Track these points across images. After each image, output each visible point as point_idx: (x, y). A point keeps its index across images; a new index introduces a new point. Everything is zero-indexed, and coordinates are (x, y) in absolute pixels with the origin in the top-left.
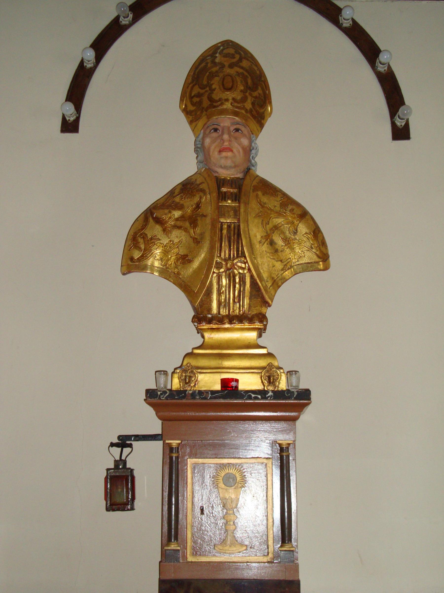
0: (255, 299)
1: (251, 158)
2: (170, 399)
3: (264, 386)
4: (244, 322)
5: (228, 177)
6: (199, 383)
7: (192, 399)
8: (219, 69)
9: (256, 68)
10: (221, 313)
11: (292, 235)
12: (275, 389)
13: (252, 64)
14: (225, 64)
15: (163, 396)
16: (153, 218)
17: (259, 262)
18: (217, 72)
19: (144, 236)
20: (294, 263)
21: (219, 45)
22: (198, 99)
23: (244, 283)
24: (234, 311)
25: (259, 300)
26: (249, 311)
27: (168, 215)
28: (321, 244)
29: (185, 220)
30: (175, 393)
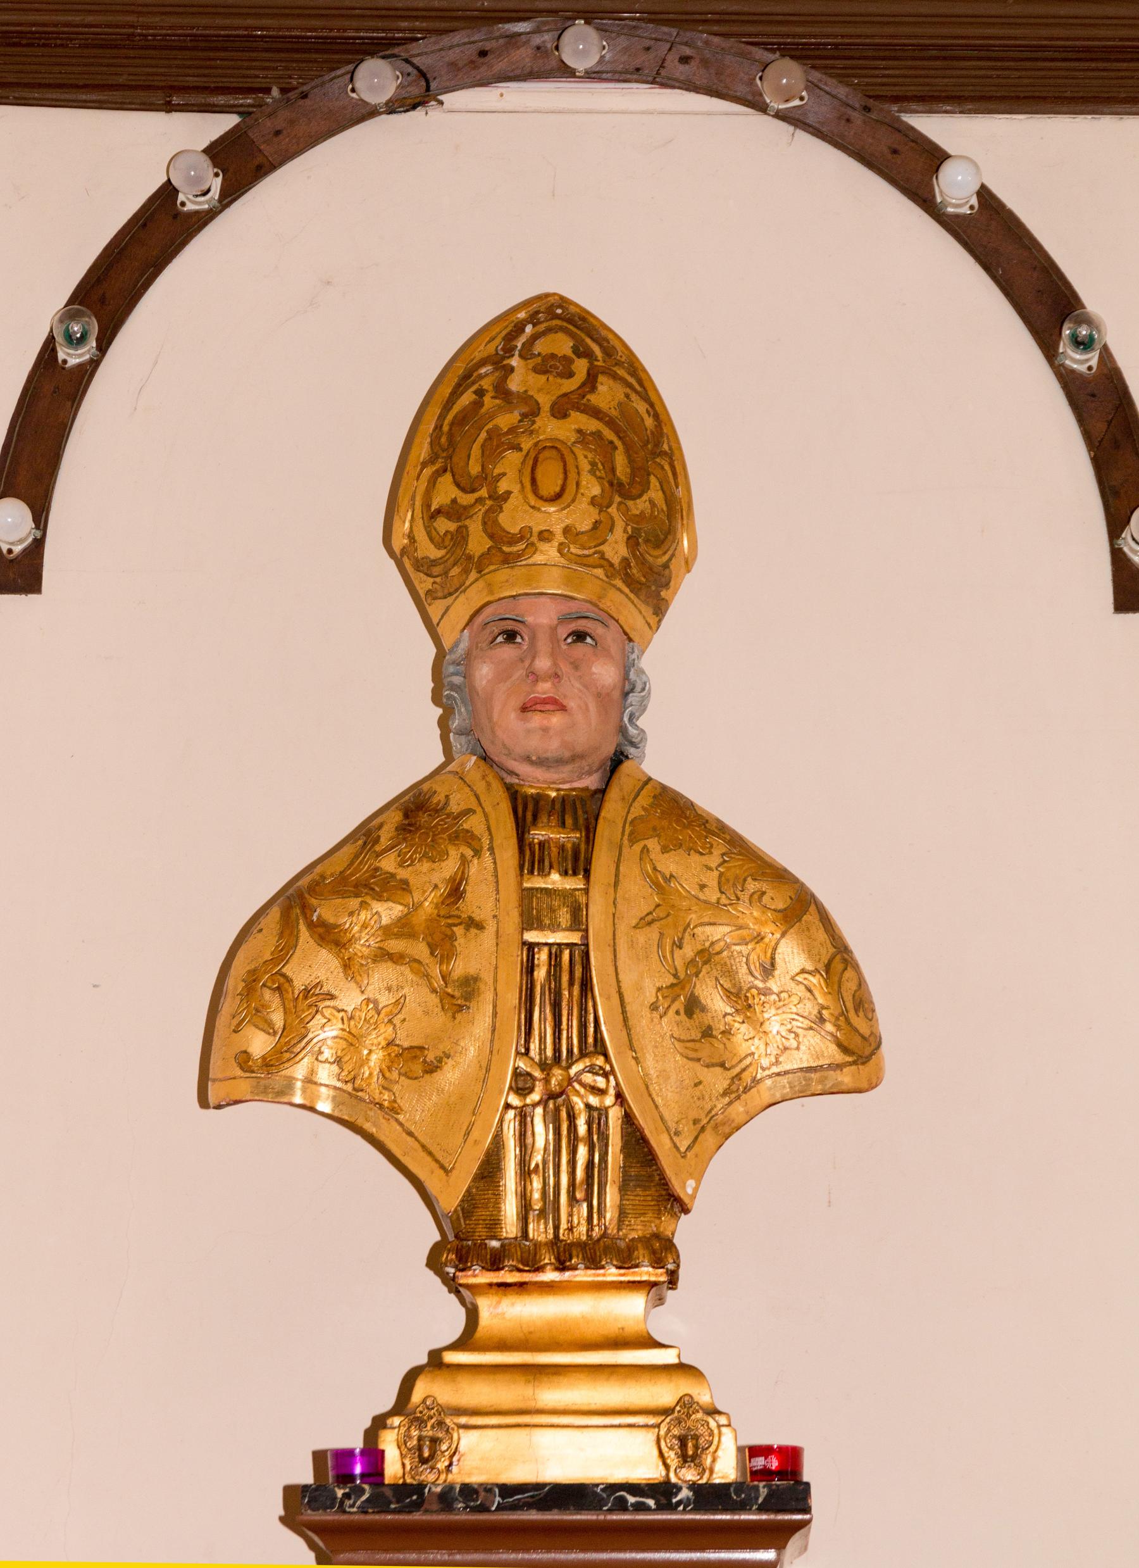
0: (639, 1191)
1: (626, 719)
2: (373, 1512)
3: (667, 1466)
4: (603, 1263)
5: (552, 789)
6: (462, 1459)
7: (442, 1510)
8: (520, 421)
9: (641, 407)
10: (531, 1236)
11: (756, 978)
12: (701, 1478)
13: (628, 390)
14: (540, 400)
15: (351, 1502)
16: (311, 925)
17: (652, 1072)
18: (512, 430)
19: (282, 984)
20: (763, 1069)
21: (522, 315)
22: (452, 526)
23: (604, 1138)
24: (570, 1229)
25: (652, 1191)
26: (619, 1229)
27: (359, 915)
28: (850, 1005)
29: (412, 935)
30: (389, 1493)
